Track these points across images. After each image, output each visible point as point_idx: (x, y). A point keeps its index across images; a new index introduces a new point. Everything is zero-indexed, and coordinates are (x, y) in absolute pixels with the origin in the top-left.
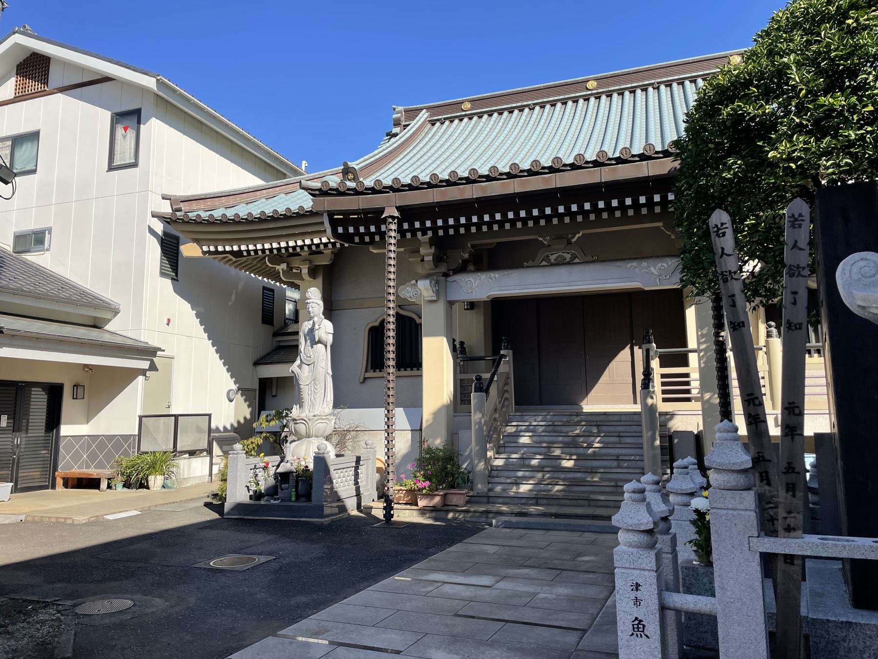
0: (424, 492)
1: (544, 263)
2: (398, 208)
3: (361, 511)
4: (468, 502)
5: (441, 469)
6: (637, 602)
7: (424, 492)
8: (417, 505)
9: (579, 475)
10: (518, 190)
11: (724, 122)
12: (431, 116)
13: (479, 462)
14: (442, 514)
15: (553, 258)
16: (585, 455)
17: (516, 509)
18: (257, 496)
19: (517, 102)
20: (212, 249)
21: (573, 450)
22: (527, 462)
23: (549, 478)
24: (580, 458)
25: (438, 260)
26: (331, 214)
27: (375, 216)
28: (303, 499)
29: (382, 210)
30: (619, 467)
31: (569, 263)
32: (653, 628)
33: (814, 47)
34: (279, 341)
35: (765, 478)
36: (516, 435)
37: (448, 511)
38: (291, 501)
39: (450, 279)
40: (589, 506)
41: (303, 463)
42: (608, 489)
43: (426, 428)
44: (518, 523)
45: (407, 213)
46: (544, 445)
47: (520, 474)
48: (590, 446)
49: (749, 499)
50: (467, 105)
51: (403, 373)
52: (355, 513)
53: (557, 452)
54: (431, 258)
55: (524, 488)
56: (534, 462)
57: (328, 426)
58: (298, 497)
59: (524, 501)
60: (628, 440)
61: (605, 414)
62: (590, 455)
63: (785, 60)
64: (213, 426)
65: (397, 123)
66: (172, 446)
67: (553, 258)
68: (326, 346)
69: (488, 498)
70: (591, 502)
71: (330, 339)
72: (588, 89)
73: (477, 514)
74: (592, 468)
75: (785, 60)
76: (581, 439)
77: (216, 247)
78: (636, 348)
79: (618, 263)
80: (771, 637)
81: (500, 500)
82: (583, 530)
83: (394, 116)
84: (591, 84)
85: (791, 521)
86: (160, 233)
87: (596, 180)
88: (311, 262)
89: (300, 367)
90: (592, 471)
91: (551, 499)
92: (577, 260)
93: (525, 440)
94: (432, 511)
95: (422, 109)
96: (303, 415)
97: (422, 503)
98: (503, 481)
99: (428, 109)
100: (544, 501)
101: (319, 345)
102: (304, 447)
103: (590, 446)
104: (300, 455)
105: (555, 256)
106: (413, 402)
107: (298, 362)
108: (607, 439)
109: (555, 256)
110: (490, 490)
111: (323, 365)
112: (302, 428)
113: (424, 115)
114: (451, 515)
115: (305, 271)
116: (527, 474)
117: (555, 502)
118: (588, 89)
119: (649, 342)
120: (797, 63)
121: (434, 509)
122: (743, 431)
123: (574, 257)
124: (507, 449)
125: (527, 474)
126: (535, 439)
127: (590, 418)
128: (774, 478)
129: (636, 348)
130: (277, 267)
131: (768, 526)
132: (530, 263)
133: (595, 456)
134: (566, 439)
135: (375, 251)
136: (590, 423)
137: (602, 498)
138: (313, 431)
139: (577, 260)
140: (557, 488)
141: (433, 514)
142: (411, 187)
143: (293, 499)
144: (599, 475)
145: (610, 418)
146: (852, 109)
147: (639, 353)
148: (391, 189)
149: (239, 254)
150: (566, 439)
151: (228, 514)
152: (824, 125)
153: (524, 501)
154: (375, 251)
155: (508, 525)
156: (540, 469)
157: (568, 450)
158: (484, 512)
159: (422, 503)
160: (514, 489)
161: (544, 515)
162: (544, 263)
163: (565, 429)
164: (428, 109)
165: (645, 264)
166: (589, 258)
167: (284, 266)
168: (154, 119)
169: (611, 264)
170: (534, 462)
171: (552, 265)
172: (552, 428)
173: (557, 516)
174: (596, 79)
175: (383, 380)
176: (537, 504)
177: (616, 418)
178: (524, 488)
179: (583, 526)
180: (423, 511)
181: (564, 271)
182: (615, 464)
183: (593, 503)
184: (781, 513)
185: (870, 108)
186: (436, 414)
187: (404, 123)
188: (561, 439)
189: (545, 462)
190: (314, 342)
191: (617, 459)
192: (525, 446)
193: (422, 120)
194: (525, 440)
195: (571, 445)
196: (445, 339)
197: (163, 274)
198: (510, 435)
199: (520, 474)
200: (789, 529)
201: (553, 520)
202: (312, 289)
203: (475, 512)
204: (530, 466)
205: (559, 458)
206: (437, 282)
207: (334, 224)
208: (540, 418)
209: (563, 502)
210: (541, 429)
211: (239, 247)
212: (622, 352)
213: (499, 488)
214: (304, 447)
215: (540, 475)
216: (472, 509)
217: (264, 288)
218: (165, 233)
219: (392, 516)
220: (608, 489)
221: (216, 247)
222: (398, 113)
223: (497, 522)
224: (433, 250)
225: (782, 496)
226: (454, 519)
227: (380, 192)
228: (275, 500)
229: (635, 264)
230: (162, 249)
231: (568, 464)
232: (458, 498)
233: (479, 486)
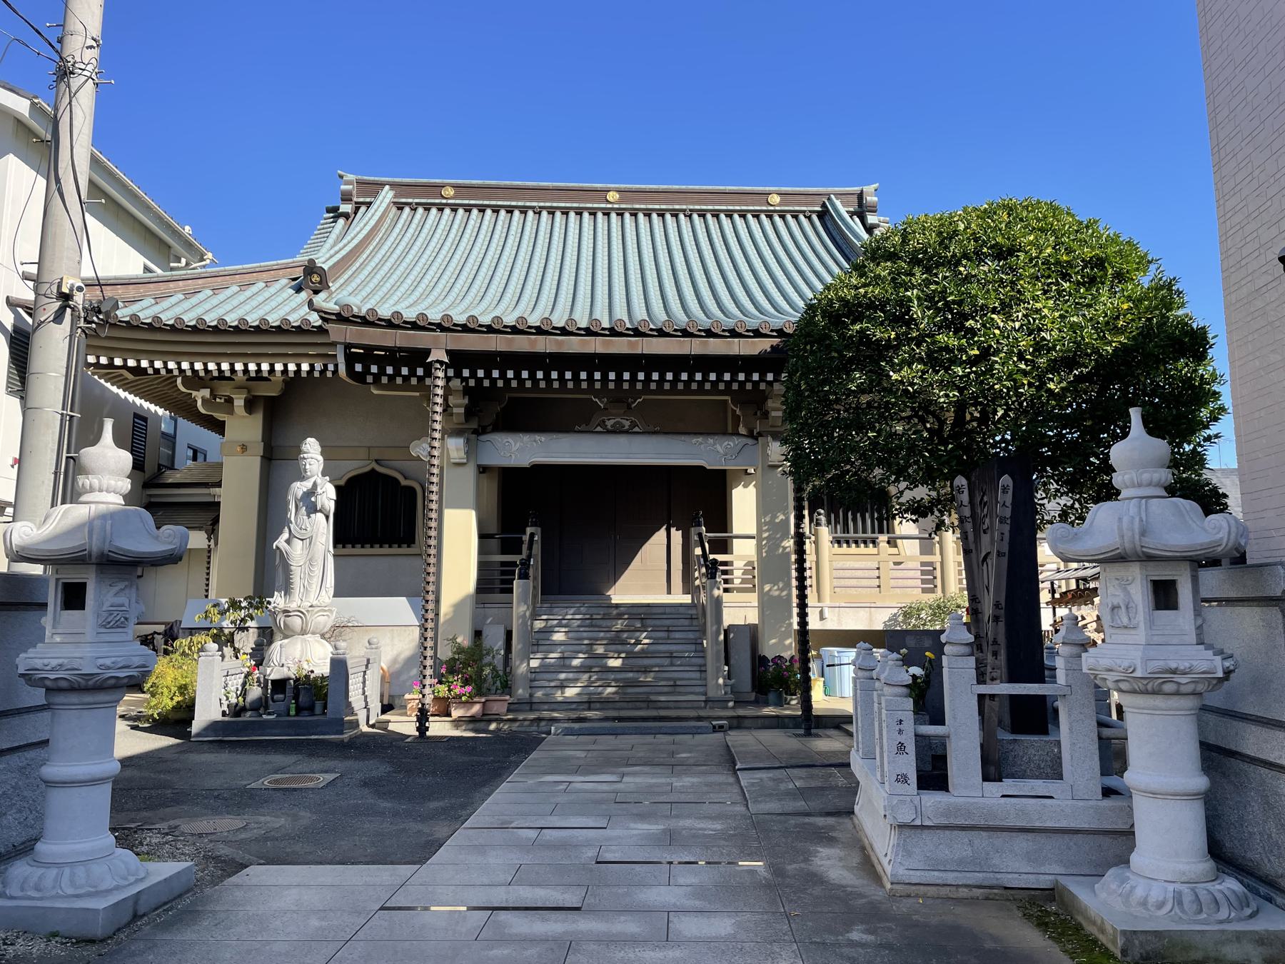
0: (464, 699)
1: (599, 429)
2: (449, 352)
3: (373, 726)
4: (509, 711)
5: (474, 668)
6: (900, 732)
7: (464, 699)
8: (449, 715)
9: (631, 675)
10: (600, 350)
11: (852, 336)
12: (395, 196)
13: (521, 663)
14: (481, 725)
15: (609, 424)
16: (632, 652)
17: (574, 715)
18: (237, 711)
19: (518, 200)
20: (104, 360)
21: (620, 647)
22: (567, 662)
23: (598, 680)
24: (630, 656)
25: (469, 413)
26: (348, 346)
27: (418, 357)
28: (306, 713)
29: (427, 352)
30: (672, 665)
31: (627, 432)
32: (911, 748)
33: (933, 287)
34: (150, 496)
35: (980, 648)
36: (548, 631)
37: (490, 721)
38: (288, 715)
39: (483, 438)
40: (648, 708)
41: (305, 666)
42: (666, 689)
43: (445, 622)
44: (580, 729)
45: (458, 359)
46: (586, 642)
47: (563, 676)
48: (638, 642)
49: (971, 661)
50: (449, 192)
51: (349, 550)
52: (365, 729)
53: (600, 650)
54: (462, 410)
55: (571, 692)
56: (576, 662)
57: (323, 621)
58: (299, 710)
59: (574, 706)
60: (677, 635)
61: (648, 605)
62: (638, 652)
63: (909, 293)
64: (814, 623)
65: (346, 198)
66: (832, 624)
67: (609, 424)
68: (327, 517)
69: (531, 704)
70: (649, 703)
71: (331, 506)
72: (608, 202)
73: (526, 723)
74: (646, 667)
75: (909, 293)
76: (625, 635)
77: (125, 361)
78: (673, 530)
79: (683, 438)
80: (982, 746)
81: (546, 707)
82: (655, 732)
83: (343, 187)
84: (612, 196)
85: (994, 675)
86: (10, 328)
87: (686, 351)
88: (249, 392)
89: (288, 542)
90: (646, 671)
91: (605, 703)
92: (636, 429)
93: (559, 637)
94: (470, 722)
95: (382, 185)
96: (293, 606)
97: (456, 713)
98: (547, 684)
99: (393, 185)
100: (598, 705)
101: (319, 515)
102: (299, 646)
103: (638, 642)
104: (302, 656)
105: (612, 422)
106: (423, 591)
107: (285, 535)
108: (653, 634)
109: (612, 422)
110: (531, 696)
111: (323, 540)
112: (296, 622)
113: (387, 195)
114: (493, 726)
115: (239, 402)
116: (571, 676)
117: (611, 705)
118: (608, 202)
119: (699, 525)
120: (919, 298)
121: (472, 720)
122: (796, 627)
123: (633, 425)
124: (541, 648)
125: (571, 676)
126: (571, 635)
127: (632, 611)
128: (985, 647)
129: (673, 530)
130: (194, 393)
131: (981, 679)
132: (583, 427)
133: (644, 654)
134: (608, 635)
135: (376, 392)
136: (633, 617)
137: (663, 698)
138: (311, 627)
139: (636, 429)
140: (610, 690)
141: (471, 726)
142: (465, 328)
143: (293, 712)
144: (652, 674)
145: (655, 611)
146: (962, 349)
147: (677, 536)
148: (440, 327)
149: (138, 371)
150: (608, 635)
151: (198, 735)
152: (937, 359)
153: (574, 706)
154: (376, 392)
155: (569, 732)
156: (584, 669)
157: (613, 647)
158: (534, 720)
159: (456, 713)
160: (559, 693)
161: (606, 719)
162: (599, 429)
163: (604, 623)
164: (393, 185)
165: (711, 441)
166: (651, 428)
167: (206, 393)
168: (11, 155)
169: (675, 437)
170: (576, 662)
171: (609, 432)
172: (590, 623)
173: (621, 719)
174: (619, 191)
175: (418, 558)
176: (589, 709)
177: (661, 610)
178: (571, 692)
179: (651, 728)
180: (457, 723)
181: (622, 440)
182: (667, 661)
183: (651, 705)
184: (989, 669)
185: (977, 352)
186: (458, 607)
187: (355, 199)
188: (602, 634)
189: (590, 662)
190: (312, 509)
191: (671, 656)
192: (561, 644)
193: (384, 205)
194: (559, 637)
195: (616, 641)
196: (474, 513)
197: (11, 393)
198: (540, 631)
199: (563, 676)
200: (993, 679)
201: (617, 724)
202: (309, 439)
203: (525, 720)
204: (570, 666)
205: (605, 657)
206: (468, 442)
207: (351, 359)
208: (572, 611)
209: (618, 705)
210: (577, 623)
211: (138, 361)
212: (657, 534)
213: (539, 694)
214: (299, 646)
215: (586, 676)
216: (521, 718)
217: (136, 416)
218: (16, 329)
219: (427, 729)
220: (666, 689)
221: (125, 361)
222: (348, 183)
223: (557, 729)
224: (466, 401)
225: (990, 658)
226: (498, 730)
227: (423, 328)
228: (269, 714)
229: (700, 439)
230: (11, 347)
231: (616, 663)
232: (499, 706)
233: (520, 691)
